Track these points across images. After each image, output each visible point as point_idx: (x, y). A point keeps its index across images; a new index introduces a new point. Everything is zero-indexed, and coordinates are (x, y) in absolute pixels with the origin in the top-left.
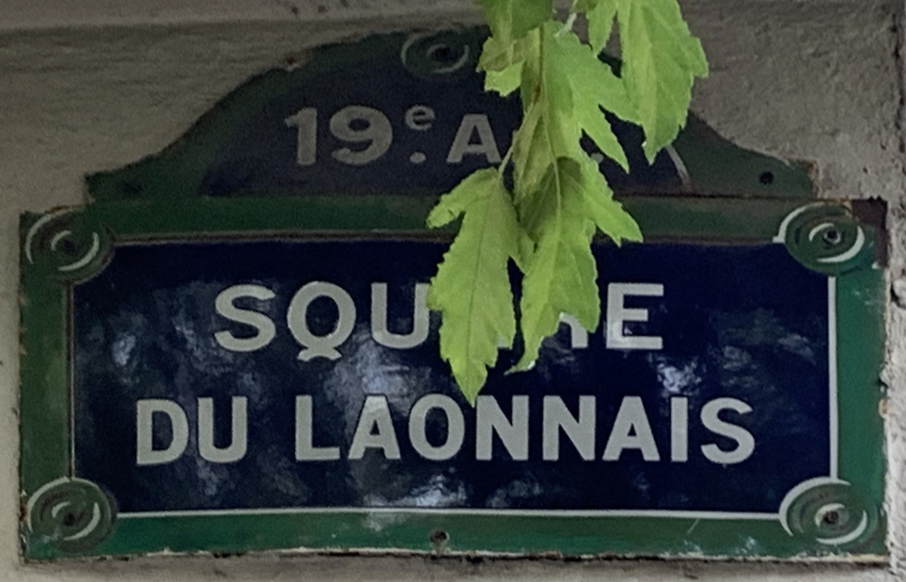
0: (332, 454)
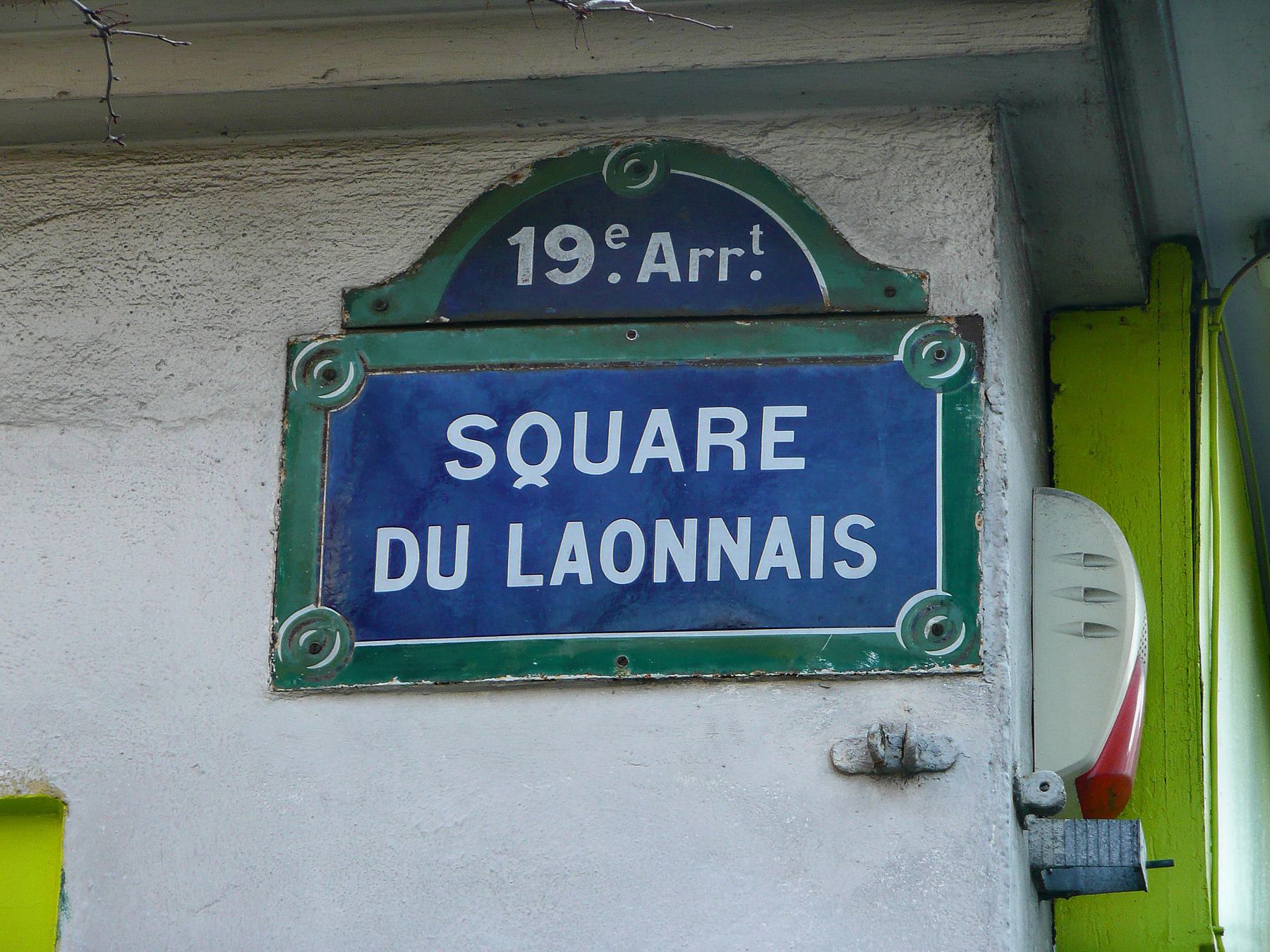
0: (537, 580)
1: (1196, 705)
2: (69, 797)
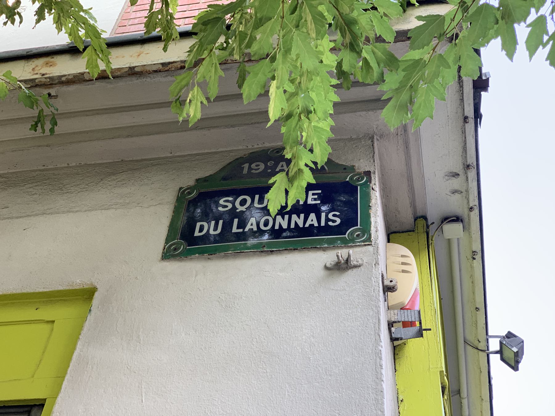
0: (241, 230)
1: (436, 322)
2: (98, 287)
